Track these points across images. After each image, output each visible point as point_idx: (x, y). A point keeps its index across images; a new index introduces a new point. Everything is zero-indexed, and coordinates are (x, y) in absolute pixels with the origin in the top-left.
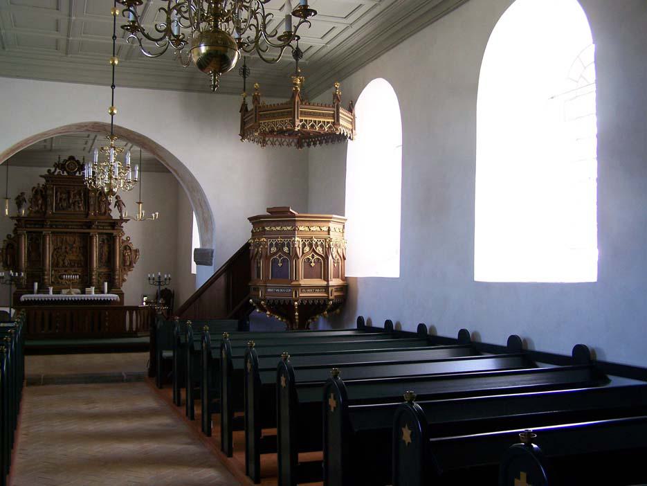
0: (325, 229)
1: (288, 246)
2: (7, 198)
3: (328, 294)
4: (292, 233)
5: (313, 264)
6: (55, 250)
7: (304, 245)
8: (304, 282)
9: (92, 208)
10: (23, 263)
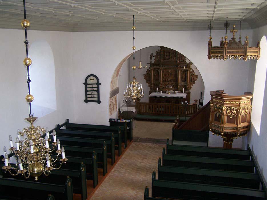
0: (238, 103)
1: (221, 109)
2: (140, 62)
3: (237, 131)
4: (222, 104)
5: (231, 118)
6: (164, 75)
7: (227, 110)
8: (226, 125)
9: (178, 59)
10: (153, 80)
